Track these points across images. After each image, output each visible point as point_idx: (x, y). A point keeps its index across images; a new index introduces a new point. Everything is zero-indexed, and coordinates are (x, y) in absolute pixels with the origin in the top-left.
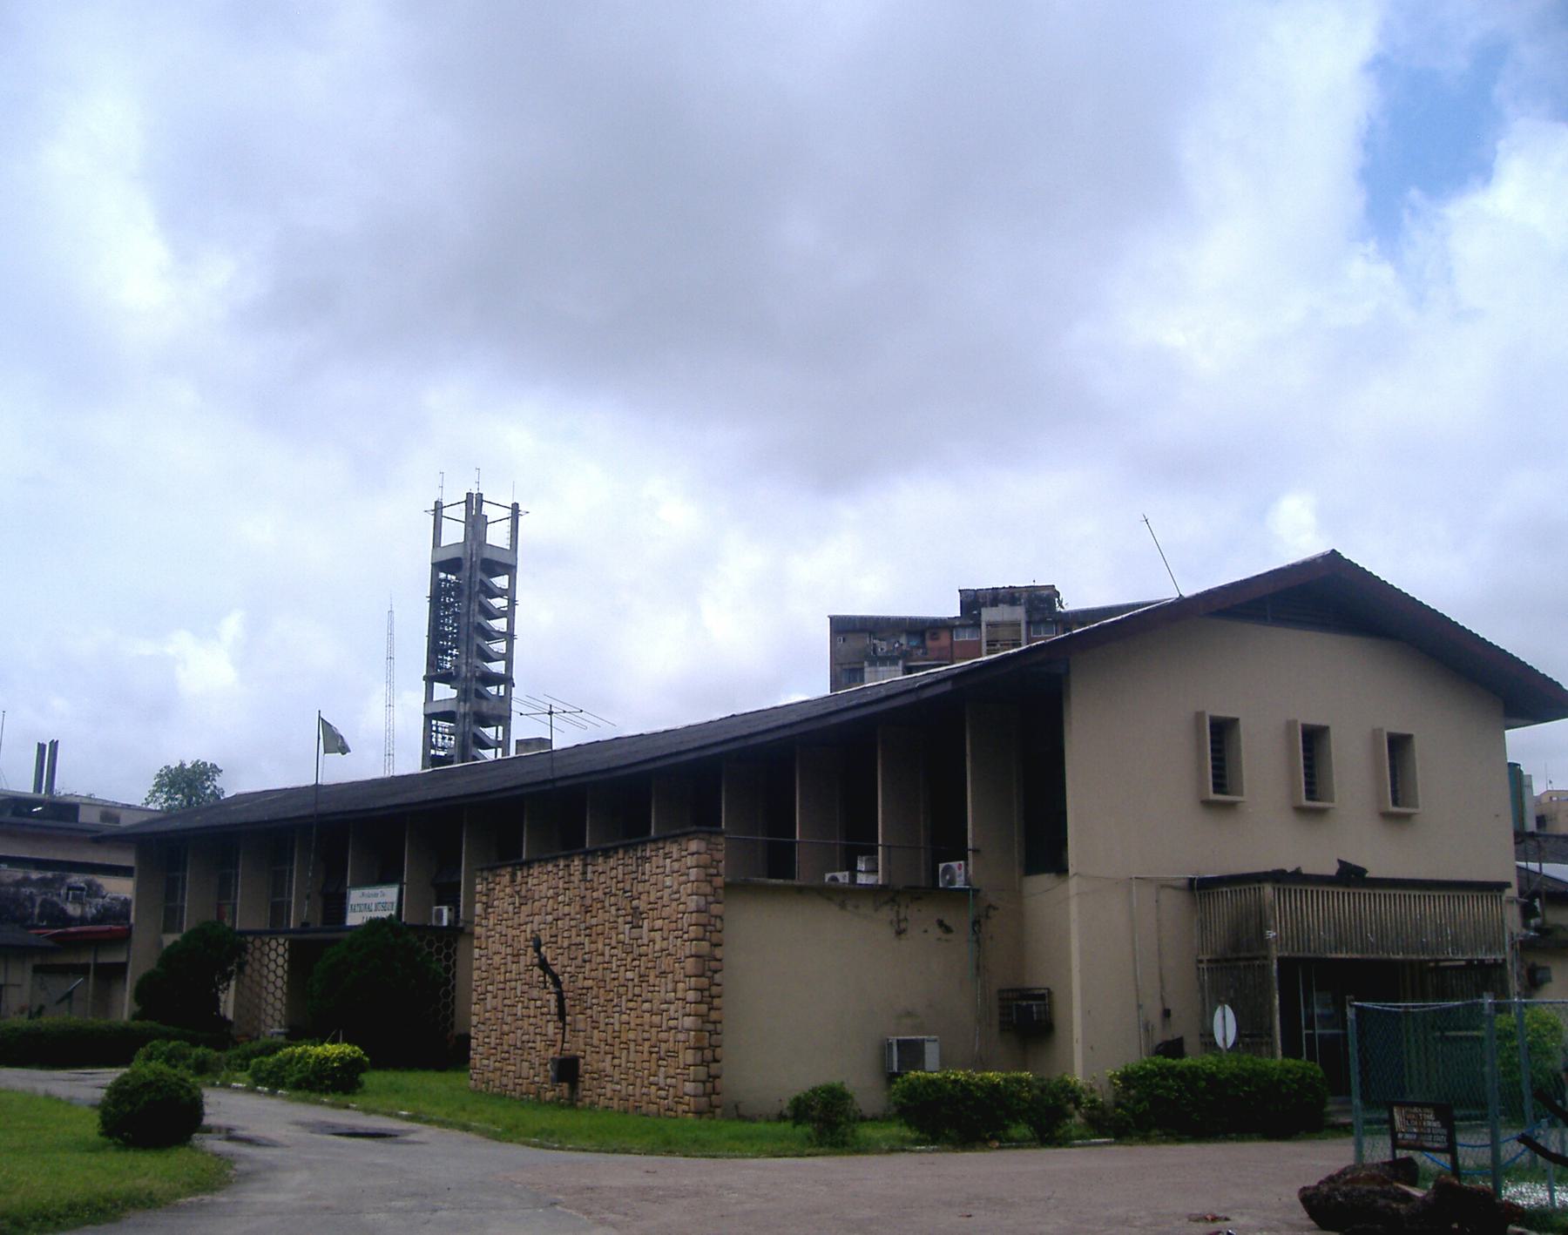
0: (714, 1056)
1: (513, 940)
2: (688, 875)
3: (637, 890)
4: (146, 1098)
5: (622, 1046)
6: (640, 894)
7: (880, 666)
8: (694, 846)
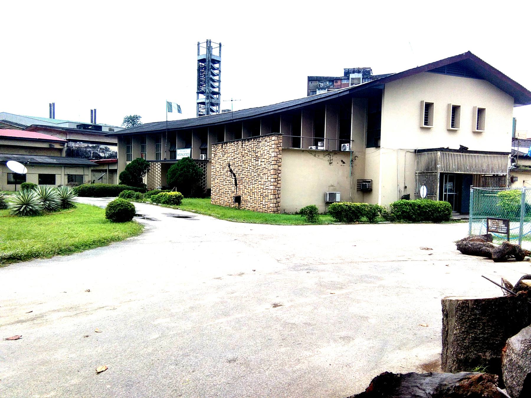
8: (273, 138)
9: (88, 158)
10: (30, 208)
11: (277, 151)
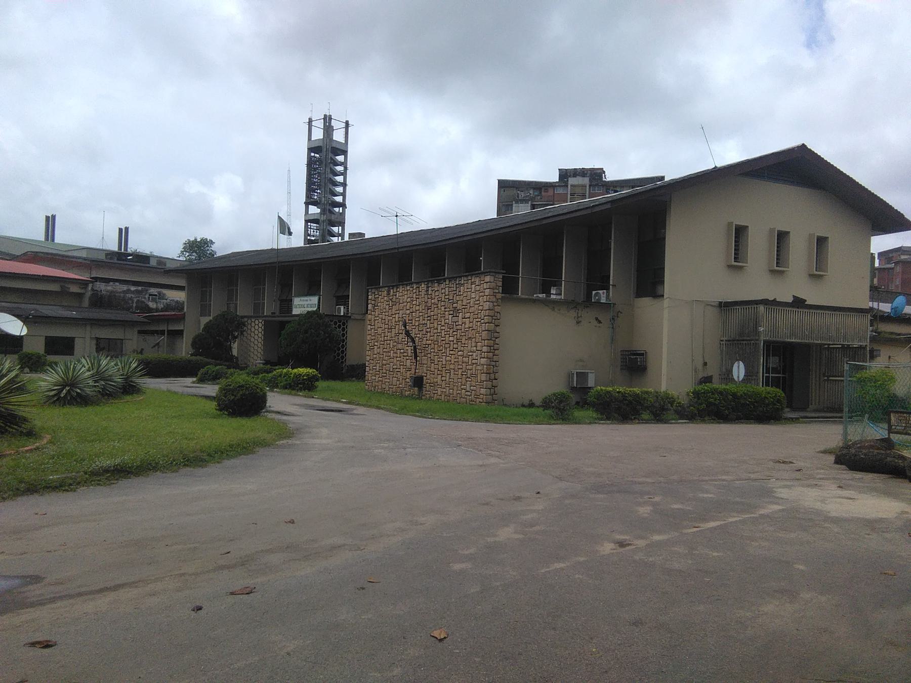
5: (447, 371)
8: (488, 279)
9: (128, 309)
10: (76, 392)
11: (494, 300)
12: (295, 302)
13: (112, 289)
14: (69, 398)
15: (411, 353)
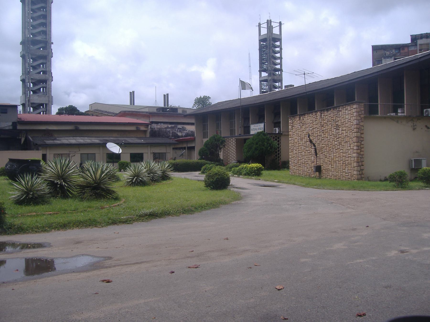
0: (362, 164)
1: (301, 135)
2: (353, 114)
3: (337, 120)
4: (216, 177)
5: (334, 162)
6: (338, 121)
7: (387, 59)
8: (355, 106)
9: (168, 137)
10: (140, 180)
12: (251, 127)
13: (160, 127)
14: (137, 183)
15: (314, 152)
